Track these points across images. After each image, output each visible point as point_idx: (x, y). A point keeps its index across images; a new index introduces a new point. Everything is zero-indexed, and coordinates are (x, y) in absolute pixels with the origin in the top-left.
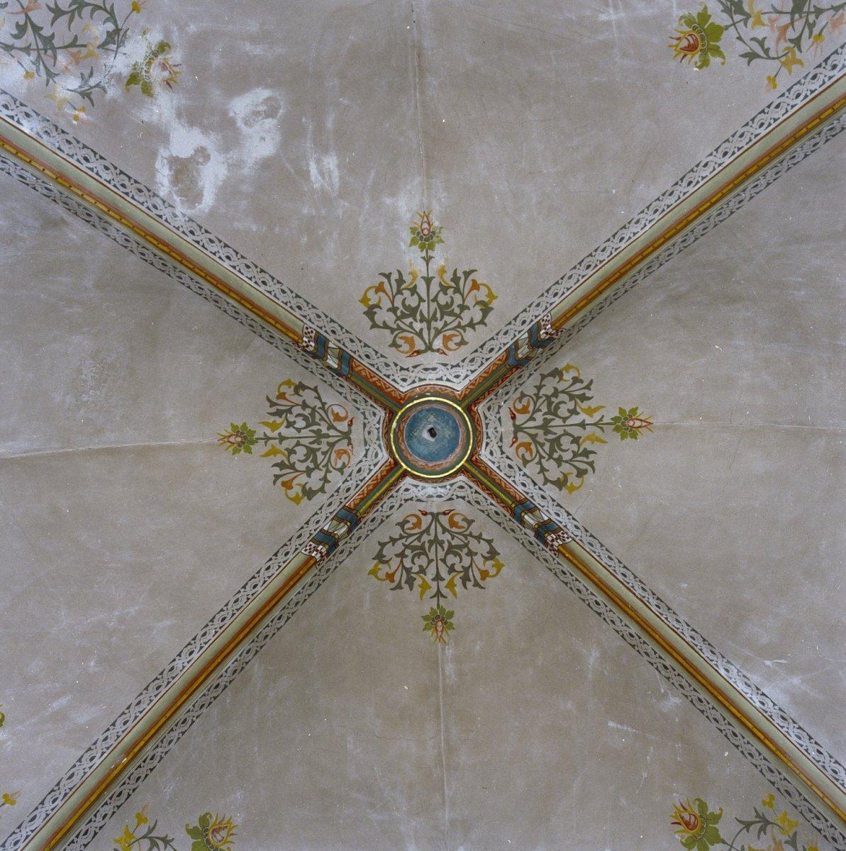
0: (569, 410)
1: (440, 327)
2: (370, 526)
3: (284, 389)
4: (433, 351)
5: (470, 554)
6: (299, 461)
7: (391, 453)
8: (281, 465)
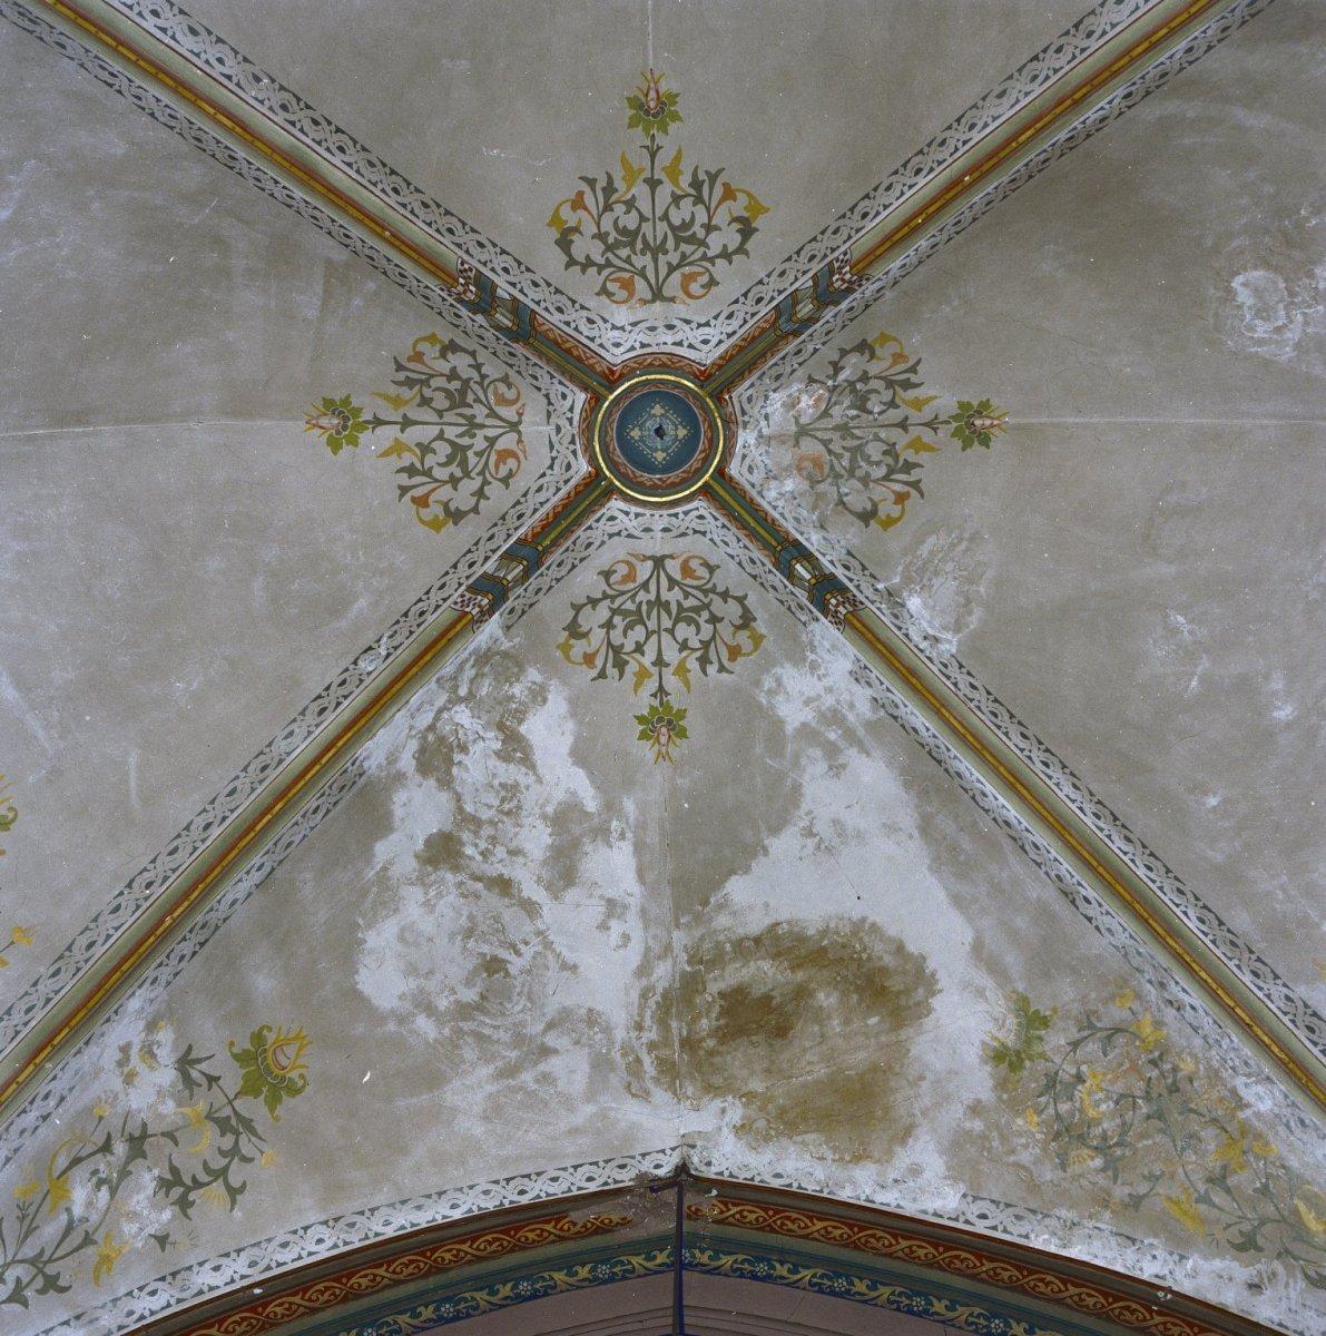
0: (434, 452)
1: (642, 592)
2: (554, 573)
3: (423, 347)
4: (652, 558)
5: (714, 620)
6: (439, 464)
7: (592, 460)
8: (411, 471)
